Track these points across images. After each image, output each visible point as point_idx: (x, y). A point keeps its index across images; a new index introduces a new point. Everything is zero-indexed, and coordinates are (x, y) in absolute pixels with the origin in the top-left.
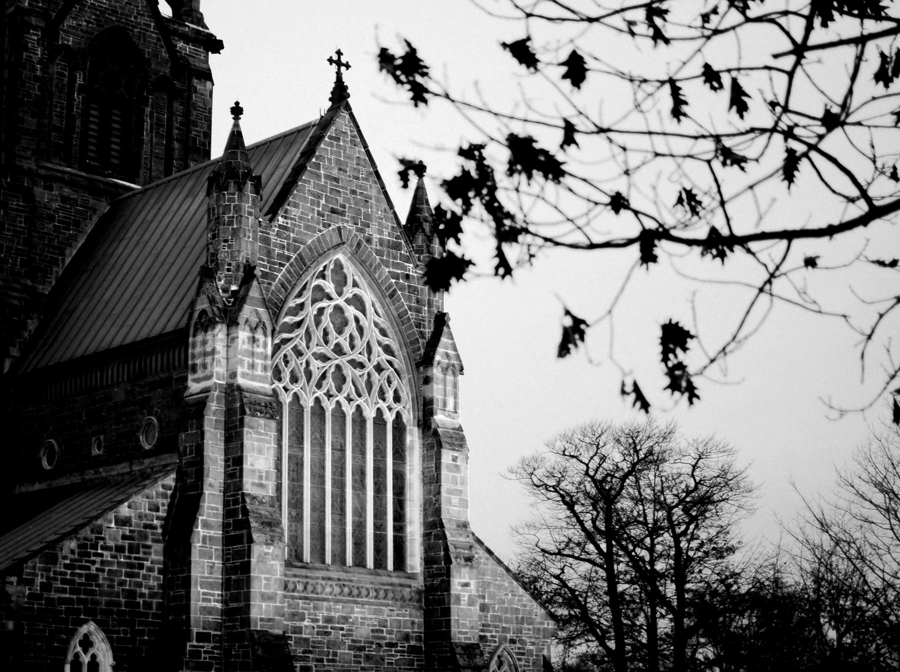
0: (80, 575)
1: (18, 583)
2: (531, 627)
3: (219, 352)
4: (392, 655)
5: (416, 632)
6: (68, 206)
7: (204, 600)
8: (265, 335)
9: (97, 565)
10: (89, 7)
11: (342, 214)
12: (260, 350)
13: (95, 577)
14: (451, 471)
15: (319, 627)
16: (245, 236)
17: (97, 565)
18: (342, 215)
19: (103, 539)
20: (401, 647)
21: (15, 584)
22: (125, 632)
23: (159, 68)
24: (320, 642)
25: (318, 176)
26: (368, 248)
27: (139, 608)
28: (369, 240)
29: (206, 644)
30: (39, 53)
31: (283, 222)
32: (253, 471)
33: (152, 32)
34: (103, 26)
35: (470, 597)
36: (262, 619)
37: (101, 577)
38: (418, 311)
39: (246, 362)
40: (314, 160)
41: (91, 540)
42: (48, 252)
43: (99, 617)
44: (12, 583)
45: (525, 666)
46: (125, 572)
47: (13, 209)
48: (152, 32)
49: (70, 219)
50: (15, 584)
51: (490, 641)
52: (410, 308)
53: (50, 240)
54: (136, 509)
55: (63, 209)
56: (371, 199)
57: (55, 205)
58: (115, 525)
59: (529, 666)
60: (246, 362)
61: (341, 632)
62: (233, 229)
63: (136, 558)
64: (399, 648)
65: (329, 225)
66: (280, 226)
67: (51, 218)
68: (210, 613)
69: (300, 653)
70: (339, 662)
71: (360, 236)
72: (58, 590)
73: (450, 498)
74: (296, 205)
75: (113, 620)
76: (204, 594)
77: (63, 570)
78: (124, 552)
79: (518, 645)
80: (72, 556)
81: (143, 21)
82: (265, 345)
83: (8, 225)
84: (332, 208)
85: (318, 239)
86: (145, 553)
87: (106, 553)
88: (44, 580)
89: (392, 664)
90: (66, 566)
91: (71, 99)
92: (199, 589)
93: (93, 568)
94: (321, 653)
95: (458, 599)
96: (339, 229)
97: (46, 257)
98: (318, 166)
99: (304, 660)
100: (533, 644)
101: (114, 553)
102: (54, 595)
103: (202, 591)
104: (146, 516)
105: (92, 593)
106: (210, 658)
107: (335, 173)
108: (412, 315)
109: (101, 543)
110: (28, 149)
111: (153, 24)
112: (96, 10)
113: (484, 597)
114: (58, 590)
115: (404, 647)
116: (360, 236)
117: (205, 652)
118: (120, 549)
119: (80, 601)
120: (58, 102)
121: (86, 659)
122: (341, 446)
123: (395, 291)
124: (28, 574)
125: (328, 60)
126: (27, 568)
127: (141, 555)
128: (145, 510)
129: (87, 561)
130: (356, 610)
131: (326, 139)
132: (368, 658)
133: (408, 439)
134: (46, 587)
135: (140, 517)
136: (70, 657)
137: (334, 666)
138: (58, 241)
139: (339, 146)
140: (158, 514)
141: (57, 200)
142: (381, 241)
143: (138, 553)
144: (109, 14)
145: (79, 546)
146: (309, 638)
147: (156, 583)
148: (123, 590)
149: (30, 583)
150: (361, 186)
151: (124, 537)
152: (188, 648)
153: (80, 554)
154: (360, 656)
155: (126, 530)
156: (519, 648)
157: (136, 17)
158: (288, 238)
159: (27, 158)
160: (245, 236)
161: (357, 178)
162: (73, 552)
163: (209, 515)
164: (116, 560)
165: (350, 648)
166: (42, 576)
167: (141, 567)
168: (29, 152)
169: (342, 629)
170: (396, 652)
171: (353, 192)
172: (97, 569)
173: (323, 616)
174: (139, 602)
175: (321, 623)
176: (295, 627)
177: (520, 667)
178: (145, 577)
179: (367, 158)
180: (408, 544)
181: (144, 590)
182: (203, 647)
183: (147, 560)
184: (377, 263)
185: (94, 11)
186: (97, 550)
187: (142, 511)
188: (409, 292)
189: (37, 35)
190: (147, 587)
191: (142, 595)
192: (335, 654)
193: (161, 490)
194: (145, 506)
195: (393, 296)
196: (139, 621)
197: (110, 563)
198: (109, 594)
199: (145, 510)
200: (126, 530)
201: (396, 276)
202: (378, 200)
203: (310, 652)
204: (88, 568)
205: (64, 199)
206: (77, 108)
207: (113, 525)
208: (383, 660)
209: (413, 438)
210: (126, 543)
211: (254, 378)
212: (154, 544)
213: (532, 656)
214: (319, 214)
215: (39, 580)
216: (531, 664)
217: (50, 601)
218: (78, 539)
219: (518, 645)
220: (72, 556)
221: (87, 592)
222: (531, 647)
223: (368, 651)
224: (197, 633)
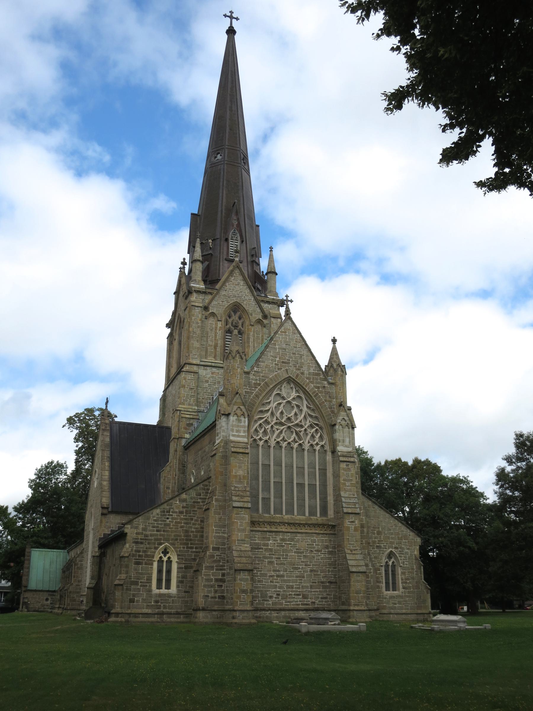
0: (161, 524)
1: (131, 528)
2: (407, 541)
3: (224, 427)
4: (319, 556)
5: (332, 545)
6: (215, 376)
7: (216, 533)
8: (245, 418)
9: (170, 520)
10: (223, 296)
11: (288, 363)
12: (242, 424)
13: (169, 525)
14: (345, 471)
15: (278, 543)
16: (236, 377)
17: (170, 520)
18: (288, 364)
19: (172, 508)
20: (323, 551)
21: (129, 528)
22: (184, 548)
23: (256, 316)
24: (278, 550)
25: (276, 349)
26: (302, 377)
27: (191, 537)
28: (303, 373)
29: (217, 552)
30: (200, 317)
31: (257, 370)
32: (236, 476)
33: (252, 302)
34: (229, 302)
35: (355, 527)
36: (238, 540)
37: (172, 525)
38: (331, 402)
39: (235, 430)
40: (273, 342)
41: (167, 509)
42: (206, 395)
43: (170, 542)
44: (128, 528)
45: (404, 559)
46: (184, 522)
47: (189, 379)
48: (252, 302)
49: (216, 381)
50: (129, 528)
51: (383, 548)
52: (326, 401)
53: (206, 390)
54: (189, 495)
55: (212, 377)
56: (304, 356)
57: (208, 376)
58: (179, 502)
59: (407, 560)
60: (235, 430)
61: (290, 545)
62: (231, 374)
63: (189, 516)
64: (323, 552)
65: (281, 369)
66: (255, 371)
67: (207, 381)
68: (219, 538)
69: (267, 555)
70: (289, 559)
71: (298, 372)
72: (150, 531)
73: (345, 483)
74: (263, 362)
75: (178, 542)
76: (216, 530)
77: (153, 522)
78: (184, 514)
79: (399, 550)
80: (158, 516)
81: (248, 298)
82: (245, 422)
83: (187, 386)
84: (282, 361)
85: (276, 375)
86: (193, 514)
87: (174, 514)
88: (144, 527)
89: (319, 559)
90: (155, 520)
91: (216, 333)
92: (214, 528)
93: (168, 520)
94: (280, 555)
95: (348, 528)
96: (287, 370)
97: (205, 397)
98: (275, 344)
99: (269, 558)
100: (408, 549)
101: (178, 514)
102: (149, 533)
103: (215, 529)
104: (194, 498)
105: (167, 531)
106: (219, 558)
107: (284, 346)
108: (327, 403)
109: (172, 510)
110: (196, 355)
111: (252, 299)
112: (226, 296)
113: (379, 528)
114: (150, 531)
115: (326, 551)
116: (298, 372)
117: (217, 555)
118: (181, 512)
119: (161, 535)
120: (211, 335)
121: (165, 559)
122: (291, 463)
123: (317, 394)
124: (136, 524)
125: (293, 301)
126: (135, 522)
127: (192, 515)
128: (194, 495)
129: (165, 518)
130: (298, 535)
131: (279, 333)
132: (305, 557)
133: (328, 458)
134: (144, 529)
135: (191, 498)
136: (156, 558)
137: (286, 560)
138: (210, 390)
139: (286, 335)
140: (200, 497)
141: (209, 374)
142: (309, 374)
143: (190, 513)
144: (232, 297)
145: (161, 512)
146: (272, 548)
147: (199, 526)
148: (182, 530)
149: (137, 528)
150: (298, 351)
151: (183, 507)
152: (208, 554)
153: (161, 515)
154: (301, 556)
155: (185, 504)
156: (400, 551)
157: (244, 297)
158: (259, 376)
159: (196, 358)
160: (236, 377)
161: (296, 347)
162: (158, 514)
163: (219, 496)
164: (179, 517)
165: (295, 552)
166: (143, 525)
167: (192, 519)
168: (196, 356)
169: (291, 544)
170: (321, 554)
171: (294, 354)
172: (170, 521)
173: (280, 539)
174: (191, 535)
175: (279, 542)
176: (265, 544)
177: (401, 560)
178: (194, 524)
179: (301, 339)
180: (329, 505)
181: (193, 530)
182: (215, 553)
183: (194, 516)
184: (307, 382)
185: (225, 297)
186: (170, 513)
187: (193, 496)
188: (325, 394)
189: (199, 309)
190: (194, 528)
191: (192, 532)
192: (287, 555)
193: (202, 486)
194: (194, 494)
195: (316, 396)
196: (190, 543)
197: (175, 519)
198: (176, 532)
199: (194, 495)
200: (185, 504)
201: (318, 388)
202: (307, 356)
203: (273, 555)
204: (166, 521)
205: (212, 373)
206: (218, 336)
207: (178, 502)
208: (314, 558)
209: (329, 457)
210: (184, 510)
211: (238, 436)
212: (198, 510)
213: (408, 555)
214: (275, 364)
215: (141, 527)
216: (407, 558)
217: (146, 536)
218: (160, 509)
219: (399, 550)
220: (158, 516)
221: (164, 531)
222: (407, 551)
223: (305, 553)
224: (212, 547)
